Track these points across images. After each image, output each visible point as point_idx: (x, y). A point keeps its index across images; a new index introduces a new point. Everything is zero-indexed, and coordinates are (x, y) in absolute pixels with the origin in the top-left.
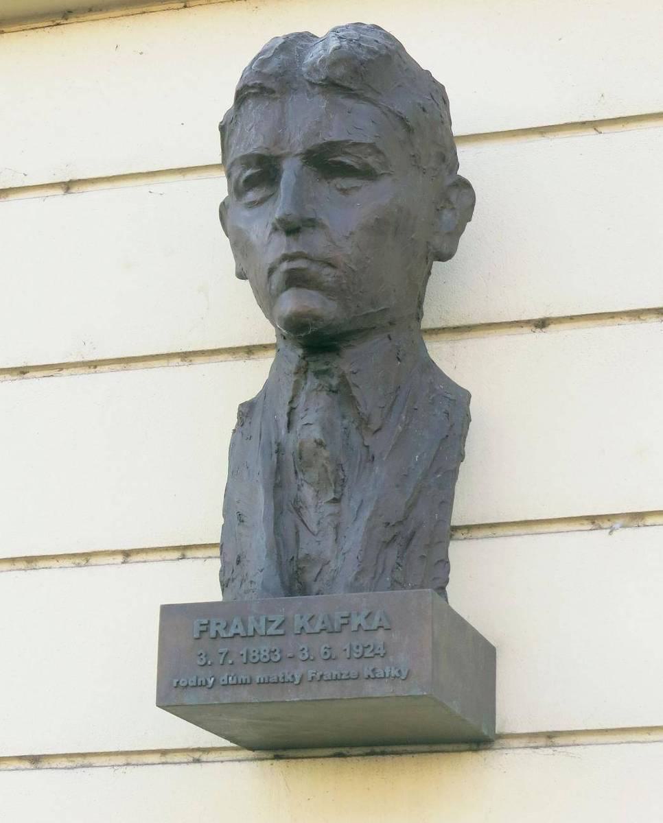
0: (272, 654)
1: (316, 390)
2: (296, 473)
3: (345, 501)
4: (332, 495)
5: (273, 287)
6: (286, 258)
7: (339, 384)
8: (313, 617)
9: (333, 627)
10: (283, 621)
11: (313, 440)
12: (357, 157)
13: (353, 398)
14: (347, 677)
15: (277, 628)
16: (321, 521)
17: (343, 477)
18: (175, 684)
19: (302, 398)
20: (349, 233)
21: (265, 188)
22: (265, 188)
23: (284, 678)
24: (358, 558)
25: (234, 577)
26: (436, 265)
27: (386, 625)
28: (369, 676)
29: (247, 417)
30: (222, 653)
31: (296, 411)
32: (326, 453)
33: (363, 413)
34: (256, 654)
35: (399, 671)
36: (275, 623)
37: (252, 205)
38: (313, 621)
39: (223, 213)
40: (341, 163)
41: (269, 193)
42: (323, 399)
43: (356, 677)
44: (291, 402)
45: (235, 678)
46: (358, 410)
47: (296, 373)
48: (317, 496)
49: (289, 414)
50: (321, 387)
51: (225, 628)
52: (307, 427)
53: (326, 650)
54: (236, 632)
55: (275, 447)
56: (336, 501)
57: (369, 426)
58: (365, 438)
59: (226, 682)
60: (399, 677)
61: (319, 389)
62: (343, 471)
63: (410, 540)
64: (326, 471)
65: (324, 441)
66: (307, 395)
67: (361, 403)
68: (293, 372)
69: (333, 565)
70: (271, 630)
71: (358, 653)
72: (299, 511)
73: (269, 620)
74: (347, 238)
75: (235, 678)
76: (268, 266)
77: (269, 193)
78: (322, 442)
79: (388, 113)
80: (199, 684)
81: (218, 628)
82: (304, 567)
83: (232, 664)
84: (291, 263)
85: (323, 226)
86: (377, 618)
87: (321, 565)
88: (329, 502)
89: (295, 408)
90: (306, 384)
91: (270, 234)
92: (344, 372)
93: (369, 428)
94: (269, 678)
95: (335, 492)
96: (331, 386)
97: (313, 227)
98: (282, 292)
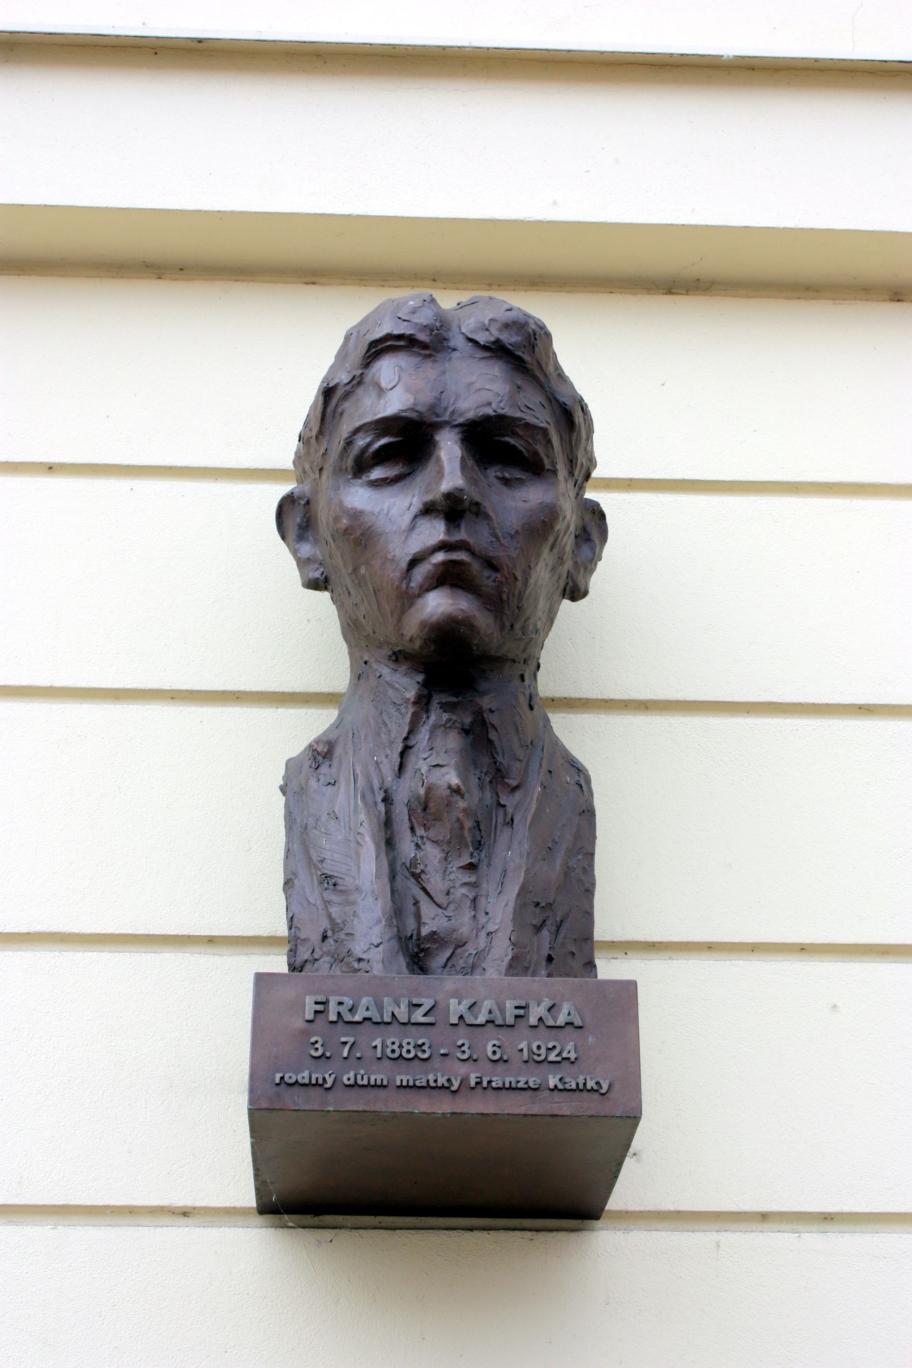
0: (419, 1049)
1: (444, 725)
2: (412, 829)
3: (483, 868)
4: (466, 860)
5: (413, 584)
6: (443, 546)
7: (472, 723)
8: (475, 1003)
9: (504, 1019)
10: (433, 1007)
11: (446, 785)
12: (527, 441)
13: (490, 742)
14: (526, 1086)
15: (425, 1015)
16: (452, 891)
17: (480, 838)
18: (278, 1081)
19: (423, 735)
20: (514, 531)
21: (401, 465)
22: (401, 465)
23: (436, 1081)
24: (510, 939)
25: (316, 957)
26: (566, 603)
27: (578, 1022)
28: (556, 1086)
29: (324, 758)
30: (345, 1043)
31: (412, 750)
32: (462, 804)
33: (501, 763)
34: (395, 1047)
35: (598, 1083)
36: (422, 1007)
37: (376, 484)
38: (475, 1009)
39: (285, 509)
40: (508, 443)
41: (405, 470)
42: (453, 741)
43: (536, 1086)
44: (406, 739)
45: (365, 1077)
46: (494, 758)
47: (415, 703)
48: (446, 859)
49: (402, 754)
50: (451, 723)
51: (350, 1010)
52: (437, 769)
53: (495, 1048)
54: (367, 1016)
55: (380, 796)
56: (471, 867)
57: (506, 781)
58: (500, 795)
59: (352, 1082)
60: (596, 1091)
61: (448, 725)
62: (480, 830)
63: (559, 927)
64: (462, 828)
65: (462, 787)
66: (432, 731)
67: (499, 750)
68: (412, 701)
69: (471, 949)
70: (418, 1016)
71: (539, 1055)
72: (420, 877)
73: (414, 1003)
74: (512, 537)
75: (365, 1077)
76: (408, 559)
77: (405, 470)
78: (460, 789)
79: (553, 400)
80: (314, 1082)
81: (341, 1009)
82: (429, 948)
83: (359, 1058)
84: (450, 553)
85: (487, 517)
86: (565, 1011)
87: (454, 946)
88: (462, 867)
89: (411, 747)
90: (428, 718)
91: (416, 517)
92: (481, 708)
93: (506, 783)
94: (415, 1081)
95: (472, 855)
96: (463, 724)
97: (477, 514)
98: (428, 590)
